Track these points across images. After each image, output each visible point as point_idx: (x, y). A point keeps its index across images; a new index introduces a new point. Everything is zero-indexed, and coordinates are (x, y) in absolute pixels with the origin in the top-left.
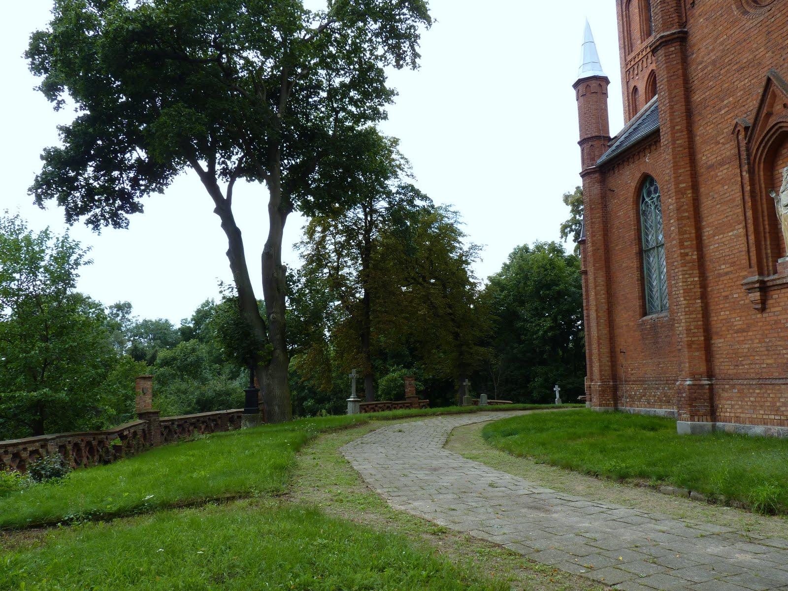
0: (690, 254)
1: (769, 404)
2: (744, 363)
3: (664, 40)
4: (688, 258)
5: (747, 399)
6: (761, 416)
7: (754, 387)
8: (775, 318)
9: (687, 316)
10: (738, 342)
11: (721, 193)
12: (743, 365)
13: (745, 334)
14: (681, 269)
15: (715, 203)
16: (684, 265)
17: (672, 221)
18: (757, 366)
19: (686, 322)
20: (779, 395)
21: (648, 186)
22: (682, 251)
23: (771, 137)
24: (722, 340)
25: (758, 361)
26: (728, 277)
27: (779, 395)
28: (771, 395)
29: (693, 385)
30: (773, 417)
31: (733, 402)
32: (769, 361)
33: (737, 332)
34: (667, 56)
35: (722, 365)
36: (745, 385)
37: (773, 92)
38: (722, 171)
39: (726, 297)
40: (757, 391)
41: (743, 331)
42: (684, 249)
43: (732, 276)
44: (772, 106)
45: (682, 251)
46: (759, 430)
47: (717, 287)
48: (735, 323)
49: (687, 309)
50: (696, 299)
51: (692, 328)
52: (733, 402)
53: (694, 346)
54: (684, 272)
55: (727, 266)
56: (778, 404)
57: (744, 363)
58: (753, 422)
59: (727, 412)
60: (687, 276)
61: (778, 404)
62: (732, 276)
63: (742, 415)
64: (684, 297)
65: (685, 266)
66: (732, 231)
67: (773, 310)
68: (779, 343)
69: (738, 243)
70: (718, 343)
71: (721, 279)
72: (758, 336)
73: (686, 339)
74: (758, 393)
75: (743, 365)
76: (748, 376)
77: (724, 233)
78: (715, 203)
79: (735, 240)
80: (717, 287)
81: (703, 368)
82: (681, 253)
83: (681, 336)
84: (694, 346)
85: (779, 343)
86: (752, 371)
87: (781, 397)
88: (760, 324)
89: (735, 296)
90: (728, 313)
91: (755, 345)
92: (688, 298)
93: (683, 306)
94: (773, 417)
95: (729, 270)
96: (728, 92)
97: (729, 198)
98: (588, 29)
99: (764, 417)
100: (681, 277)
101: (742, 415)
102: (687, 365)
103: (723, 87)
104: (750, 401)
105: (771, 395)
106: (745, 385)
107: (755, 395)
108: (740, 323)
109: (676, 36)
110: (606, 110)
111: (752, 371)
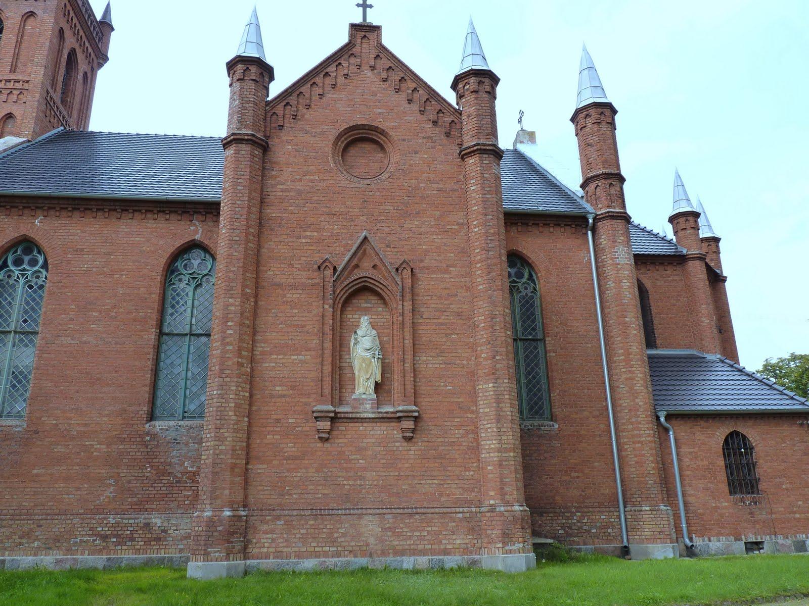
0: (245, 365)
1: (324, 535)
2: (293, 492)
3: (254, 139)
4: (243, 369)
5: (295, 532)
6: (312, 549)
7: (308, 518)
8: (339, 449)
9: (235, 435)
10: (289, 470)
11: (288, 315)
12: (291, 495)
13: (299, 462)
14: (235, 379)
15: (278, 322)
16: (238, 376)
17: (230, 324)
18: (310, 496)
19: (233, 441)
20: (339, 526)
21: (19, 252)
22: (240, 360)
23: (353, 286)
24: (265, 466)
25: (312, 491)
26: (283, 400)
27: (339, 526)
28: (328, 526)
29: (234, 516)
30: (328, 549)
31: (275, 536)
32: (326, 492)
33: (287, 459)
34: (237, 152)
35: (262, 493)
36: (295, 516)
37: (365, 250)
38: (293, 294)
39: (278, 420)
40: (312, 522)
41: (296, 458)
42: (241, 358)
43: (288, 399)
44: (360, 260)
45: (240, 360)
46: (309, 564)
47: (266, 408)
48: (285, 450)
49: (236, 427)
50: (244, 416)
51: (238, 448)
52: (275, 536)
53: (236, 470)
54: (238, 384)
55: (284, 388)
56: (336, 535)
57: (293, 492)
58: (299, 555)
59: (264, 547)
60: (240, 389)
61: (336, 535)
62: (288, 399)
63: (285, 550)
64: (235, 412)
65: (240, 378)
66: (298, 355)
67: (336, 441)
68: (340, 474)
69: (303, 369)
70: (258, 468)
71: (273, 400)
72: (315, 465)
73: (229, 461)
74: (313, 525)
75: (291, 495)
76: (295, 507)
77: (285, 355)
78: (278, 322)
79: (300, 365)
80: (266, 408)
81: (240, 497)
82: (238, 362)
83: (222, 457)
84: (236, 470)
85: (340, 474)
86: (302, 501)
87: (341, 528)
88: (320, 453)
89: (291, 421)
90: (278, 437)
91: (310, 474)
92: (238, 414)
93: (232, 422)
94: (328, 549)
95: (285, 392)
96: (312, 226)
97: (295, 323)
98: (678, 176)
99: (317, 549)
100: (234, 388)
101: (285, 550)
102: (227, 492)
103: (307, 219)
104: (299, 533)
105: (328, 526)
106: (295, 516)
107: (308, 526)
108: (293, 449)
109: (249, 137)
110: (720, 259)
111: (302, 501)
